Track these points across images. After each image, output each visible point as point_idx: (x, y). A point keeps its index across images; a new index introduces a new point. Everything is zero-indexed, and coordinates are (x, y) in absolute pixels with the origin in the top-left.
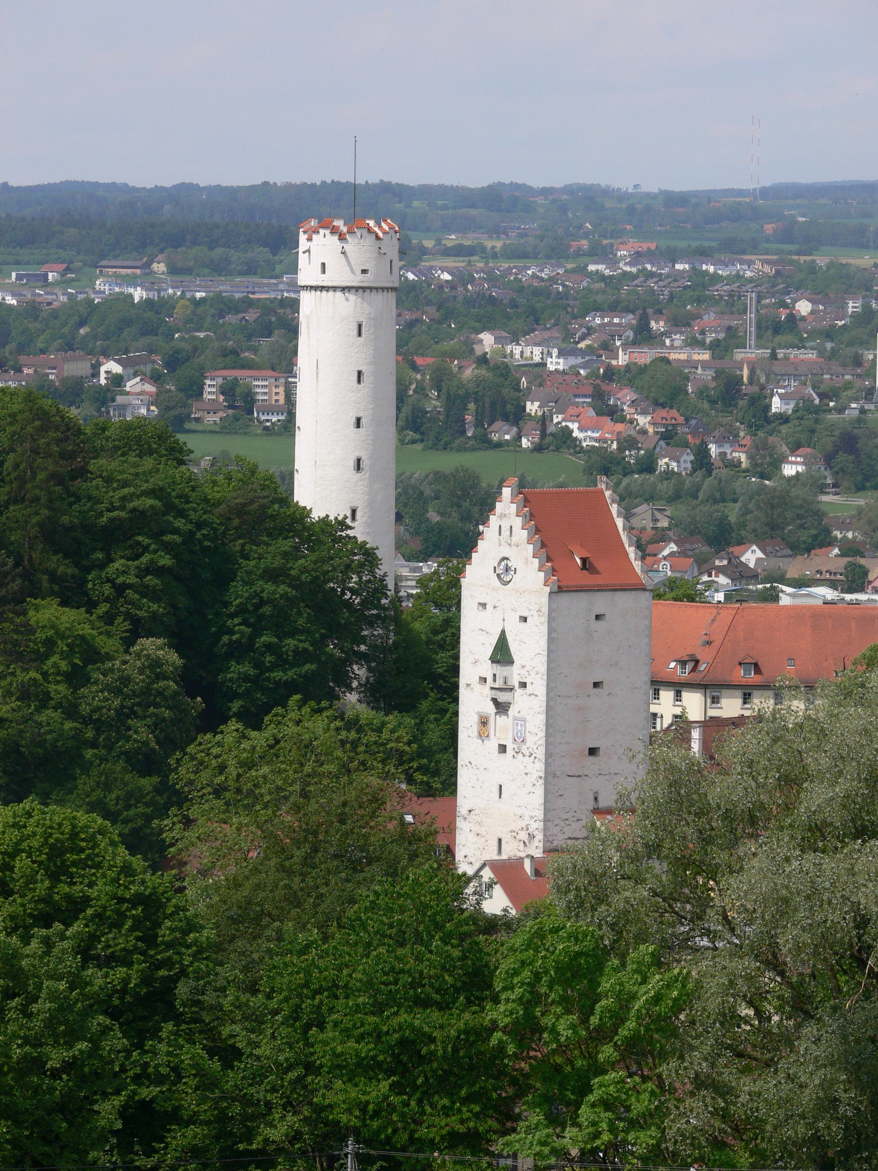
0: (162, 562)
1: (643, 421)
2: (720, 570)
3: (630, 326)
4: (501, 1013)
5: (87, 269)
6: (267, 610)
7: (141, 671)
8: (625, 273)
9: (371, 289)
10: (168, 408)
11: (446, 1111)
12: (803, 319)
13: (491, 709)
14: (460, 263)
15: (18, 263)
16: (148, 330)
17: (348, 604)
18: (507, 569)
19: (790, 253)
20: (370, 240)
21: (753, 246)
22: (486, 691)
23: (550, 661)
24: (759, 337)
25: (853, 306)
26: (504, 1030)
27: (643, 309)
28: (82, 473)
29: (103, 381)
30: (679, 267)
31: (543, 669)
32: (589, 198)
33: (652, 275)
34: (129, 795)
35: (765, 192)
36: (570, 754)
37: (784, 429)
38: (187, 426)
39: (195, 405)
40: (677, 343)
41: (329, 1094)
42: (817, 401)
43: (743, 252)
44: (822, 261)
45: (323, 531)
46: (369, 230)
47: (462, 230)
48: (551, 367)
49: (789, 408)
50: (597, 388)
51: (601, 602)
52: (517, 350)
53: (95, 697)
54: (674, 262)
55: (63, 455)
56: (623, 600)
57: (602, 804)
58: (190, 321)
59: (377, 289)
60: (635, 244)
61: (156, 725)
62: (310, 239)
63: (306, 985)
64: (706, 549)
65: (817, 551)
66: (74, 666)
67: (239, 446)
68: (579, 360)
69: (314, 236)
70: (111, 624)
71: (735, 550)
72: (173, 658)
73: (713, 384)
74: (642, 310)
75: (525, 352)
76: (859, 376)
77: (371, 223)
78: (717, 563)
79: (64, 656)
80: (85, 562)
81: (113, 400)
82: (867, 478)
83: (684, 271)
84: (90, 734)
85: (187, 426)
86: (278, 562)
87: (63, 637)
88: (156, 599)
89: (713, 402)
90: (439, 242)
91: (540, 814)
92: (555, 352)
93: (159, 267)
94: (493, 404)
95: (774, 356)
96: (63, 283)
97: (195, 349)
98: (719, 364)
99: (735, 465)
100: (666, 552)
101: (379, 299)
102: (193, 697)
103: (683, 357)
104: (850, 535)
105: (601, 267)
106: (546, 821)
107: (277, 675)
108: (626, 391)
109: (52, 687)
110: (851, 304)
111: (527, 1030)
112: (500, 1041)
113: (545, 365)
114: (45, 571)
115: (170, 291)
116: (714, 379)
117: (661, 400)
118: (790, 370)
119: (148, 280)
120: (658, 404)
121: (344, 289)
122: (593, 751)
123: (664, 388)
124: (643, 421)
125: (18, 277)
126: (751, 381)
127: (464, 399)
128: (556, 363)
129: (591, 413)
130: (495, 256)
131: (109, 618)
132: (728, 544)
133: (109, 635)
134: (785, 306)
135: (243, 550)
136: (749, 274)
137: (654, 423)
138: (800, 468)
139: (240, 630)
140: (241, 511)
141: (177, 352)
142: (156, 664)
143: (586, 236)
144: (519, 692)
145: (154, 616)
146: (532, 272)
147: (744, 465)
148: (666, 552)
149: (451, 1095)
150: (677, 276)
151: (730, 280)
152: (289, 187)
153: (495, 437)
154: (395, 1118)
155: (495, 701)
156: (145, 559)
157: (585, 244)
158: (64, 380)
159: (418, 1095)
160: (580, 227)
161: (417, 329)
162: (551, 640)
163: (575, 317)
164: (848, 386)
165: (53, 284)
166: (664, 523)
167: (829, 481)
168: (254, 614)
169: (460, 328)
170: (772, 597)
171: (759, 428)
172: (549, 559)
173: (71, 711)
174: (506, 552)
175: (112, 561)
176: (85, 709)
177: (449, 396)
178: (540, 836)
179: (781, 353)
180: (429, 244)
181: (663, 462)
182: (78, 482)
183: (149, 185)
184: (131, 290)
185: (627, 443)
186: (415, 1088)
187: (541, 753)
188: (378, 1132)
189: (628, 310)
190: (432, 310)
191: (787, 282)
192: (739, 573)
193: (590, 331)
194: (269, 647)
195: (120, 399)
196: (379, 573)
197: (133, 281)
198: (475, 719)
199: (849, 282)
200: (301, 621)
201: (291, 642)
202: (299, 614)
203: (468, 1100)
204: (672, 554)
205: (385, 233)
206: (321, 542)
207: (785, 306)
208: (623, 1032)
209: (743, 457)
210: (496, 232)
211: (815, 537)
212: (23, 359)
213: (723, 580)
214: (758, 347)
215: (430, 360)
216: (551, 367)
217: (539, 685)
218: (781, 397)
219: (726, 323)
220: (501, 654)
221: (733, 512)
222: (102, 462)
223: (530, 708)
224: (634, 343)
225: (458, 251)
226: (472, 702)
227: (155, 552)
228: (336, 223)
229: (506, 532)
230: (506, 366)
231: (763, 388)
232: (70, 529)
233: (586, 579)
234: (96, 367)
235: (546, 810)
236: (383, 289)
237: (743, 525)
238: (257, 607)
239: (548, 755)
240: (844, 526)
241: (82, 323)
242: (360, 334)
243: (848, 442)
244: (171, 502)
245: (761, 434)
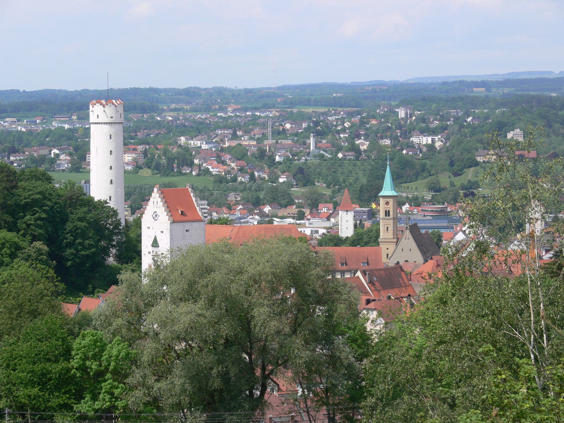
1: (233, 165)
2: (256, 214)
3: (230, 134)
4: (75, 363)
5: (50, 119)
6: (79, 231)
7: (34, 253)
8: (230, 116)
9: (114, 123)
10: (74, 165)
11: (58, 397)
12: (288, 130)
14: (175, 114)
15: (27, 117)
16: (70, 138)
17: (108, 229)
18: (156, 215)
19: (286, 108)
20: (113, 107)
21: (273, 106)
22: (150, 257)
24: (272, 136)
25: (304, 125)
26: (77, 369)
27: (234, 128)
28: (16, 187)
29: (53, 156)
30: (248, 113)
32: (220, 91)
33: (239, 116)
35: (279, 88)
37: (280, 166)
38: (81, 170)
39: (83, 163)
40: (246, 139)
41: (18, 392)
42: (291, 157)
43: (270, 108)
44: (295, 110)
45: (99, 205)
46: (113, 104)
47: (177, 103)
48: (203, 148)
49: (282, 160)
50: (217, 154)
51: (188, 226)
52: (192, 142)
54: (246, 112)
55: (8, 181)
56: (195, 225)
58: (84, 135)
59: (116, 123)
60: (234, 106)
62: (93, 107)
63: (11, 357)
64: (252, 207)
65: (289, 207)
66: (12, 251)
67: (74, 177)
68: (213, 145)
69: (95, 106)
70: (25, 237)
71: (261, 207)
72: (46, 248)
73: (256, 152)
74: (234, 128)
75: (195, 143)
76: (305, 148)
77: (114, 101)
78: (256, 211)
79: (8, 248)
80: (16, 217)
81: (56, 162)
82: (307, 182)
83: (249, 115)
85: (81, 170)
86: (82, 215)
87: (8, 242)
88: (41, 228)
89: (256, 158)
90: (168, 107)
92: (204, 143)
93: (74, 117)
94: (183, 161)
95: (277, 142)
96: (42, 123)
97: (84, 144)
98: (259, 145)
99: (264, 179)
100: (238, 209)
101: (117, 126)
102: (52, 261)
103: (247, 143)
104: (300, 201)
105: (222, 114)
107: (83, 253)
108: (227, 155)
109: (4, 259)
110: (304, 124)
111: (83, 369)
112: (75, 372)
113: (201, 147)
114: (3, 220)
115: (78, 125)
116: (257, 150)
117: (239, 158)
118: (282, 147)
119: (71, 122)
120: (238, 159)
121: (105, 123)
123: (240, 154)
124: (233, 165)
125: (27, 122)
126: (269, 151)
127: (174, 159)
128: (205, 147)
129: (216, 163)
130: (187, 111)
131: (24, 235)
132: (260, 205)
133: (24, 241)
134: (282, 126)
135: (71, 212)
136: (271, 115)
137: (236, 166)
138: (285, 180)
139: (70, 238)
140: (71, 198)
141: (78, 146)
142: (39, 250)
143: (218, 104)
145: (40, 234)
146: (200, 116)
147: (266, 179)
148: (238, 209)
149: (59, 392)
150: (247, 117)
151: (264, 117)
152: (119, 90)
153: (184, 172)
154: (40, 400)
156: (37, 215)
157: (217, 106)
158: (39, 156)
159: (48, 392)
160: (216, 101)
161: (160, 136)
162: (171, 239)
163: (212, 131)
164: (301, 152)
165: (38, 124)
166: (239, 199)
167: (295, 183)
168: (75, 233)
169: (174, 135)
170: (271, 222)
171: (272, 166)
172: (170, 212)
175: (26, 216)
177: (168, 158)
179: (279, 141)
180: (165, 108)
181: (239, 179)
182: (14, 190)
183: (73, 90)
184: (64, 125)
185: (229, 172)
186: (48, 390)
188: (35, 405)
189: (230, 128)
190: (164, 130)
191: (284, 117)
192: (262, 215)
193: (217, 135)
194: (80, 243)
195: (58, 162)
197: (65, 122)
199: (303, 117)
200: (90, 234)
202: (90, 232)
203: (65, 393)
204: (240, 209)
205: (118, 104)
206: (98, 208)
207: (282, 126)
208: (111, 368)
209: (266, 176)
210: (188, 103)
211: (288, 202)
212: (25, 149)
213: (257, 217)
214: (272, 139)
215: (162, 146)
216: (203, 148)
218: (279, 156)
219: (262, 132)
220: (155, 244)
221: (262, 195)
222: (22, 183)
224: (232, 139)
225: (175, 110)
227: (40, 213)
228: (102, 101)
230: (188, 148)
231: (273, 153)
232: (11, 206)
233: (183, 218)
234: (50, 151)
236: (118, 123)
237: (264, 199)
238: (76, 230)
240: (298, 198)
241: (47, 137)
242: (111, 138)
243: (301, 170)
244: (45, 196)
245: (272, 168)
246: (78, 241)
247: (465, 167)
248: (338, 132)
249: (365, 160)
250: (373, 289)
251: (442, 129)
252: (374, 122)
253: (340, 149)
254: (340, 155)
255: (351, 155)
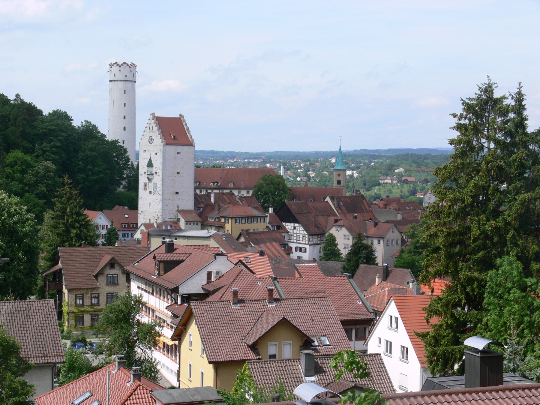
0: (57, 144)
13: (147, 181)
21: (260, 158)
23: (163, 165)
31: (161, 168)
34: (35, 205)
36: (171, 194)
51: (179, 149)
53: (29, 178)
57: (180, 209)
61: (47, 186)
66: (23, 169)
84: (27, 188)
86: (93, 146)
91: (161, 211)
106: (162, 213)
107: (92, 177)
122: (177, 193)
144: (155, 175)
155: (148, 178)
162: (163, 159)
173: (21, 181)
174: (151, 134)
176: (25, 181)
178: (161, 218)
187: (161, 193)
194: (90, 169)
196: (127, 155)
198: (143, 184)
201: (96, 168)
217: (160, 173)
220: (150, 164)
223: (157, 179)
226: (142, 179)
229: (151, 129)
235: (163, 210)
239: (163, 193)
246: (89, 167)
247: (372, 186)
248: (297, 169)
249: (313, 182)
250: (340, 212)
251: (357, 168)
252: (318, 164)
253: (299, 176)
254: (298, 179)
255: (304, 179)
